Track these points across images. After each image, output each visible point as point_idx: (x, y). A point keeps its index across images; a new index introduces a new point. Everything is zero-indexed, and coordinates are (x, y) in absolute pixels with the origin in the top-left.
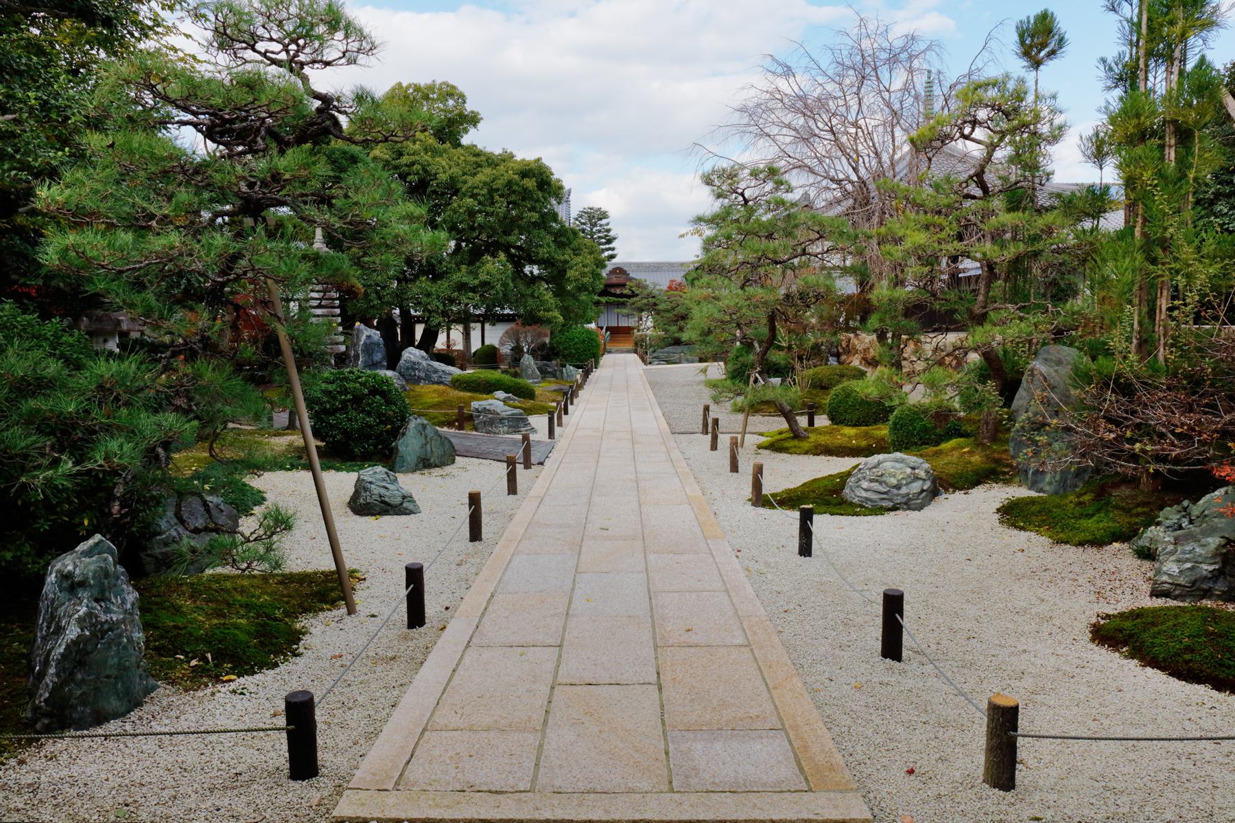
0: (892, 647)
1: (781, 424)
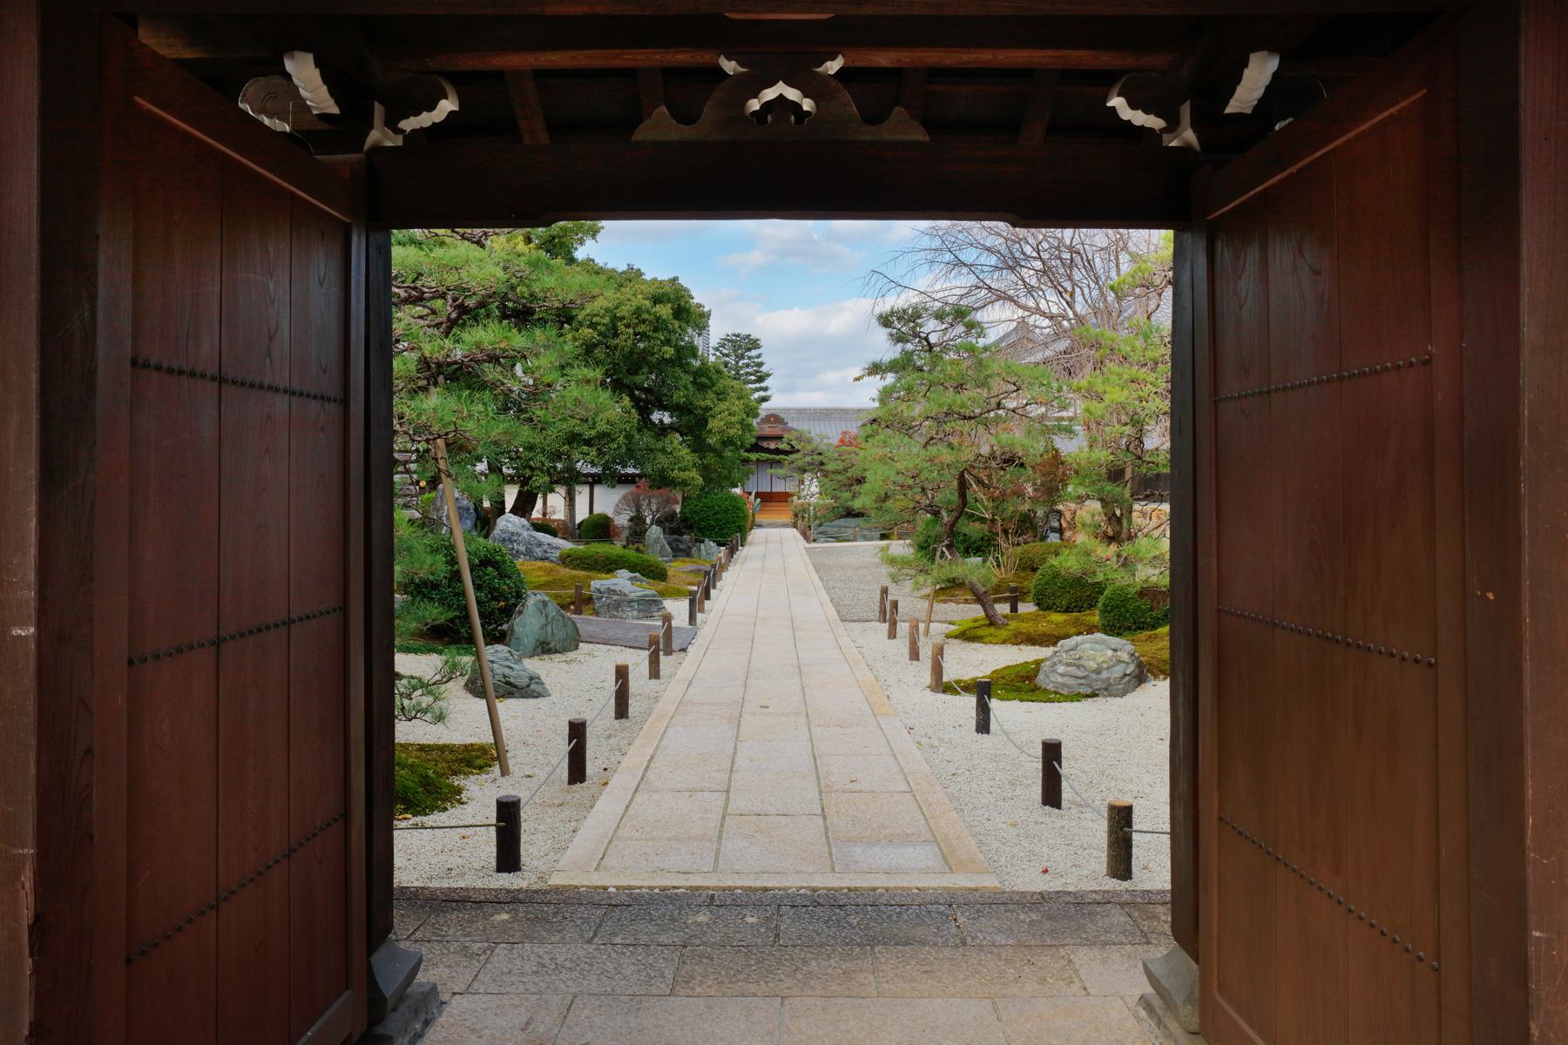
0: (1052, 794)
1: (976, 611)
